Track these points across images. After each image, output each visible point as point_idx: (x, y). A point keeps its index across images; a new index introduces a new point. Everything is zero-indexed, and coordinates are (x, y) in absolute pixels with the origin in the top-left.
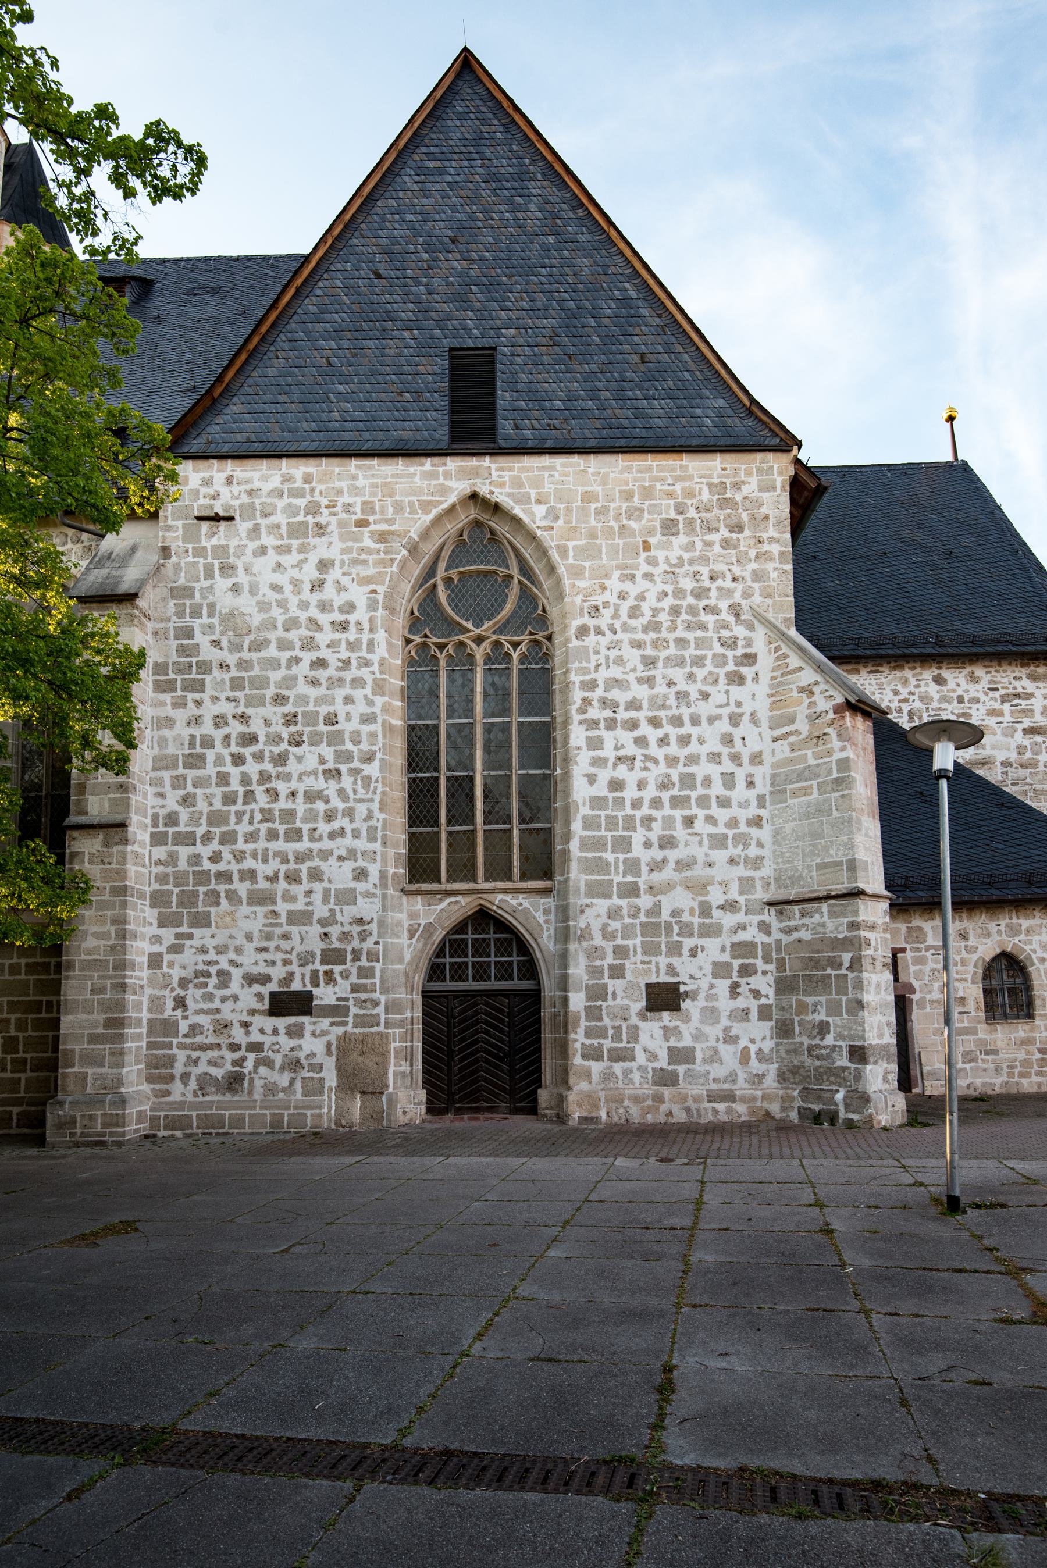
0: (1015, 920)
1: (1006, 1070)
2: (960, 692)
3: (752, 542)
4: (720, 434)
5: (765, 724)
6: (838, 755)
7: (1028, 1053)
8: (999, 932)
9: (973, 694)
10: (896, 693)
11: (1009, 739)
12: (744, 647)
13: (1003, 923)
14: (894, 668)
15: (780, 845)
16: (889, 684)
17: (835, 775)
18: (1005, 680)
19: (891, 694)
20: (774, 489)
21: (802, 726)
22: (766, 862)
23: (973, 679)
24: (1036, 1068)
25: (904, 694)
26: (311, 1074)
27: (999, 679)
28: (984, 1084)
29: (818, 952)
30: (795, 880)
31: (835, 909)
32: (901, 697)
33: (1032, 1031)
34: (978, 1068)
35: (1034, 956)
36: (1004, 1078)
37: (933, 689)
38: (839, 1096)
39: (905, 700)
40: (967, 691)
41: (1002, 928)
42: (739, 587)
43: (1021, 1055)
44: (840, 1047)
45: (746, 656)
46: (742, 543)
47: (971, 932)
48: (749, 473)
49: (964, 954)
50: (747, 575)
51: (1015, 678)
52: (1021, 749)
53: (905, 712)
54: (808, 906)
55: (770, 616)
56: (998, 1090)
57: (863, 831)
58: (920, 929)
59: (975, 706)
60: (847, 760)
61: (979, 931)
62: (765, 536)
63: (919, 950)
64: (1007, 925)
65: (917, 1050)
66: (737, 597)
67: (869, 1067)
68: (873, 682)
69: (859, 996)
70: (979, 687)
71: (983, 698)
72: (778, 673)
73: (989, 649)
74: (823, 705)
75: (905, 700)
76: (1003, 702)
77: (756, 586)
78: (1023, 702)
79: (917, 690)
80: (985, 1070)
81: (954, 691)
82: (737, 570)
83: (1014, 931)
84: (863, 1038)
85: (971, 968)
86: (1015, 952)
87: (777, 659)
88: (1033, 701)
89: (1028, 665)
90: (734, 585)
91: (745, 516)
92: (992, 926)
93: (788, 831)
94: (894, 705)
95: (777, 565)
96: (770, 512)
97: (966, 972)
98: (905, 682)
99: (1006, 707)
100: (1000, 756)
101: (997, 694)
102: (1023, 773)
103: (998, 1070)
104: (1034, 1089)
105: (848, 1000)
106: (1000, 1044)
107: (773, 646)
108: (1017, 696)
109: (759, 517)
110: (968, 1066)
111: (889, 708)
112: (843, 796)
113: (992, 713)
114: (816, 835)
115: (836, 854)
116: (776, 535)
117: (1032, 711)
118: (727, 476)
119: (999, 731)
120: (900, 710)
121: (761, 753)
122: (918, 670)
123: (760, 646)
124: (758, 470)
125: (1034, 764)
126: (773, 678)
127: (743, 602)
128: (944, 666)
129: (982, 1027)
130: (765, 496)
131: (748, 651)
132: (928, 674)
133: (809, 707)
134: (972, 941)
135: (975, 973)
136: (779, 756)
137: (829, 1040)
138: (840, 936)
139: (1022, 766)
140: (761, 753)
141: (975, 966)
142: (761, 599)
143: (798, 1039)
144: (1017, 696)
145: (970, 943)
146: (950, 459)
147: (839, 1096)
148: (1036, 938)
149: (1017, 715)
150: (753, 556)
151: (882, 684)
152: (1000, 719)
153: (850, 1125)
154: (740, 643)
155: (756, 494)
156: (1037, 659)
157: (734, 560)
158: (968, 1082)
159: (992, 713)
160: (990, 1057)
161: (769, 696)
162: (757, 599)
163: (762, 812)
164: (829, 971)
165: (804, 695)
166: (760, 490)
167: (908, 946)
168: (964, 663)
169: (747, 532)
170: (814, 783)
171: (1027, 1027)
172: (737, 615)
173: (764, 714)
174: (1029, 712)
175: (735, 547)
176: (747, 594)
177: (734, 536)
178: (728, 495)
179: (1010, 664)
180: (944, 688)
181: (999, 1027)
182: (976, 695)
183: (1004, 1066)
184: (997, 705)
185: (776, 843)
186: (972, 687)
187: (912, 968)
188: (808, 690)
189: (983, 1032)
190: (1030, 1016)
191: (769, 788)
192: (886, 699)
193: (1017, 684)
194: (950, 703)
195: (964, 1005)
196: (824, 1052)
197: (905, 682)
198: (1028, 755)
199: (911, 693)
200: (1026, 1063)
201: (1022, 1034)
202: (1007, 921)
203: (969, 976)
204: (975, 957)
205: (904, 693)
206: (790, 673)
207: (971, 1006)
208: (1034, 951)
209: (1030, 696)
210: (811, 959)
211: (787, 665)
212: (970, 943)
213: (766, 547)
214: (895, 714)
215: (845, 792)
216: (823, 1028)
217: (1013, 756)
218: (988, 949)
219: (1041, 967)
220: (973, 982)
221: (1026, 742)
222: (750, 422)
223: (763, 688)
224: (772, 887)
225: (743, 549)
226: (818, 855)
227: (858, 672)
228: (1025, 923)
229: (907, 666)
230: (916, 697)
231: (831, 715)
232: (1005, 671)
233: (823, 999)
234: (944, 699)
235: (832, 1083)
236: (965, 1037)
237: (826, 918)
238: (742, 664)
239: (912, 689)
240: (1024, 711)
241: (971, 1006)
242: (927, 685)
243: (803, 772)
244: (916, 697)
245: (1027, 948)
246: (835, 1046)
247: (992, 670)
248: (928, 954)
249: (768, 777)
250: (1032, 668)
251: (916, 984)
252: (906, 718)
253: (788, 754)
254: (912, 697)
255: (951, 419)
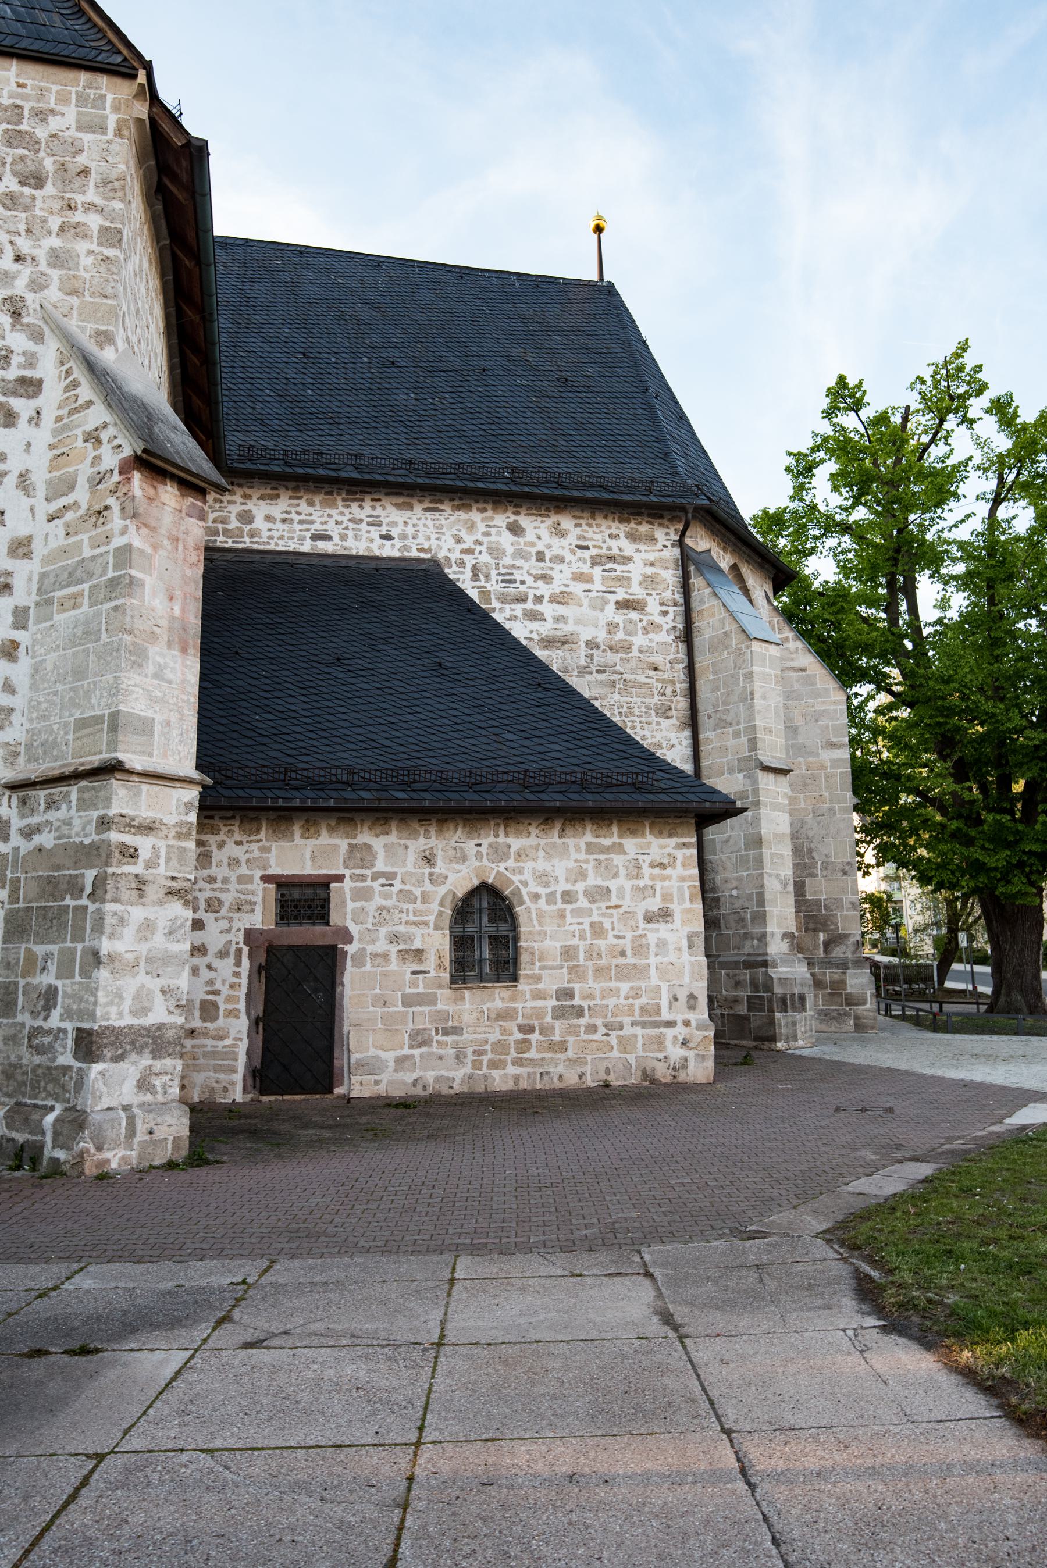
0: (502, 839)
1: (471, 1057)
2: (540, 547)
3: (57, 205)
4: (23, 32)
5: (41, 492)
6: (118, 542)
7: (504, 1031)
8: (479, 856)
9: (557, 551)
10: (458, 540)
11: (598, 613)
12: (20, 366)
13: (485, 842)
14: (458, 508)
15: (37, 690)
16: (450, 527)
17: (111, 574)
18: (599, 537)
19: (451, 542)
20: (103, 130)
21: (81, 495)
22: (16, 718)
23: (559, 532)
24: (513, 1054)
25: (469, 543)
26: (445, 1038)
27: (590, 535)
28: (437, 1079)
29: (58, 868)
30: (49, 746)
31: (86, 795)
32: (465, 546)
33: (513, 999)
34: (431, 1054)
35: (524, 891)
36: (468, 1069)
37: (506, 540)
38: (50, 1119)
39: (469, 551)
40: (549, 546)
41: (484, 849)
42: (25, 271)
43: (494, 1036)
44: (65, 1031)
45: (22, 381)
46: (39, 203)
47: (440, 854)
48: (63, 99)
49: (428, 886)
50: (42, 255)
51: (610, 536)
52: (611, 628)
53: (469, 566)
54: (56, 791)
55: (73, 324)
56: (457, 1088)
57: (151, 669)
58: (368, 847)
59: (558, 567)
60: (128, 548)
61: (451, 852)
62: (79, 199)
63: (362, 878)
64: (490, 846)
65: (346, 1028)
66: (20, 287)
67: (97, 1067)
68: (430, 523)
69: (96, 943)
70: (564, 542)
71: (569, 557)
72: (64, 412)
73: (576, 493)
74: (110, 460)
75: (469, 551)
76: (594, 564)
77: (55, 274)
78: (619, 568)
79: (485, 540)
80: (441, 1058)
81: (533, 545)
82: (24, 245)
83: (500, 854)
84: (92, 1016)
85: (435, 907)
86: (498, 884)
87: (67, 389)
88: (630, 567)
89: (628, 521)
90: (17, 266)
91: (49, 164)
92: (470, 847)
93: (49, 666)
94: (455, 556)
95: (94, 247)
96: (93, 165)
97: (427, 913)
98: (471, 527)
99: (598, 570)
100: (585, 634)
101: (587, 554)
102: (611, 657)
103: (459, 1057)
104: (509, 1086)
105: (83, 950)
106: (467, 1019)
107: (64, 368)
108: (611, 558)
109: (73, 169)
110: (416, 1052)
111: (448, 559)
112: (116, 608)
113: (578, 577)
114: (79, 673)
115: (98, 706)
116: (98, 201)
117: (629, 579)
118: (26, 98)
119: (586, 602)
120: (461, 564)
121: (29, 539)
122: (489, 513)
123: (48, 368)
124: (79, 96)
125: (627, 648)
126: (59, 419)
127: (29, 297)
128: (523, 511)
129: (444, 993)
130: (87, 138)
131: (28, 373)
132: (501, 519)
133: (93, 464)
134: (440, 867)
135: (440, 914)
136: (53, 544)
137: (54, 1021)
138: (87, 841)
139: (611, 649)
140: (29, 539)
141: (441, 904)
142: (60, 295)
143: (19, 1019)
144: (611, 558)
145: (437, 870)
146: (594, 277)
147: (50, 1119)
148: (529, 865)
149: (610, 583)
150: (55, 228)
151: (441, 527)
152: (588, 586)
153: (56, 1170)
154: (16, 360)
155: (73, 132)
156: (639, 514)
157: (22, 228)
158: (415, 1076)
159: (578, 577)
160: (449, 1039)
161: (52, 447)
162: (53, 294)
163: (20, 636)
164: (69, 901)
165: (89, 445)
166: (79, 128)
167: (347, 873)
168: (548, 510)
169: (49, 189)
170: (86, 586)
171: (506, 994)
172: (16, 315)
173: (40, 478)
174: (624, 581)
175: (26, 209)
176: (37, 285)
177: (27, 191)
178: (24, 127)
179: (606, 517)
180: (521, 540)
181: (467, 993)
182: (561, 552)
183: (469, 1051)
184: (586, 568)
185: (34, 687)
186: (556, 542)
187: (351, 906)
188: (93, 438)
189: (445, 1000)
190: (515, 978)
191: (34, 598)
192: (445, 548)
193: (613, 543)
194: (527, 560)
195: (421, 961)
196: (47, 1040)
197: (471, 527)
198: (620, 635)
199: (478, 542)
200: (501, 1047)
201: (499, 1004)
202: (492, 839)
203: (431, 919)
204: (442, 890)
205: (469, 542)
206: (77, 410)
207: (430, 963)
208: (525, 884)
209: (627, 560)
210: (50, 880)
211: (77, 397)
212: (437, 870)
213: (78, 217)
214: (455, 568)
215: (118, 602)
216: (49, 997)
217: (602, 636)
218: (461, 879)
219: (533, 907)
220: (437, 928)
221: (619, 619)
222: (78, 25)
223: (43, 435)
224: (21, 759)
225: (38, 213)
226: (78, 706)
227: (411, 507)
228: (515, 843)
229: (475, 506)
230: (483, 548)
231: (116, 477)
232: (598, 526)
233: (54, 948)
234: (519, 554)
235: (49, 1095)
236: (418, 1009)
237: (73, 812)
238: (15, 394)
239: (480, 538)
240: (619, 579)
241: (430, 963)
242: (499, 534)
243: (75, 570)
244: (483, 548)
245: (516, 878)
246: (60, 1030)
247: (583, 522)
248: (376, 885)
249: (35, 578)
250: (633, 525)
251: (354, 929)
252: (469, 574)
253: (62, 541)
254: (478, 548)
255: (599, 229)
